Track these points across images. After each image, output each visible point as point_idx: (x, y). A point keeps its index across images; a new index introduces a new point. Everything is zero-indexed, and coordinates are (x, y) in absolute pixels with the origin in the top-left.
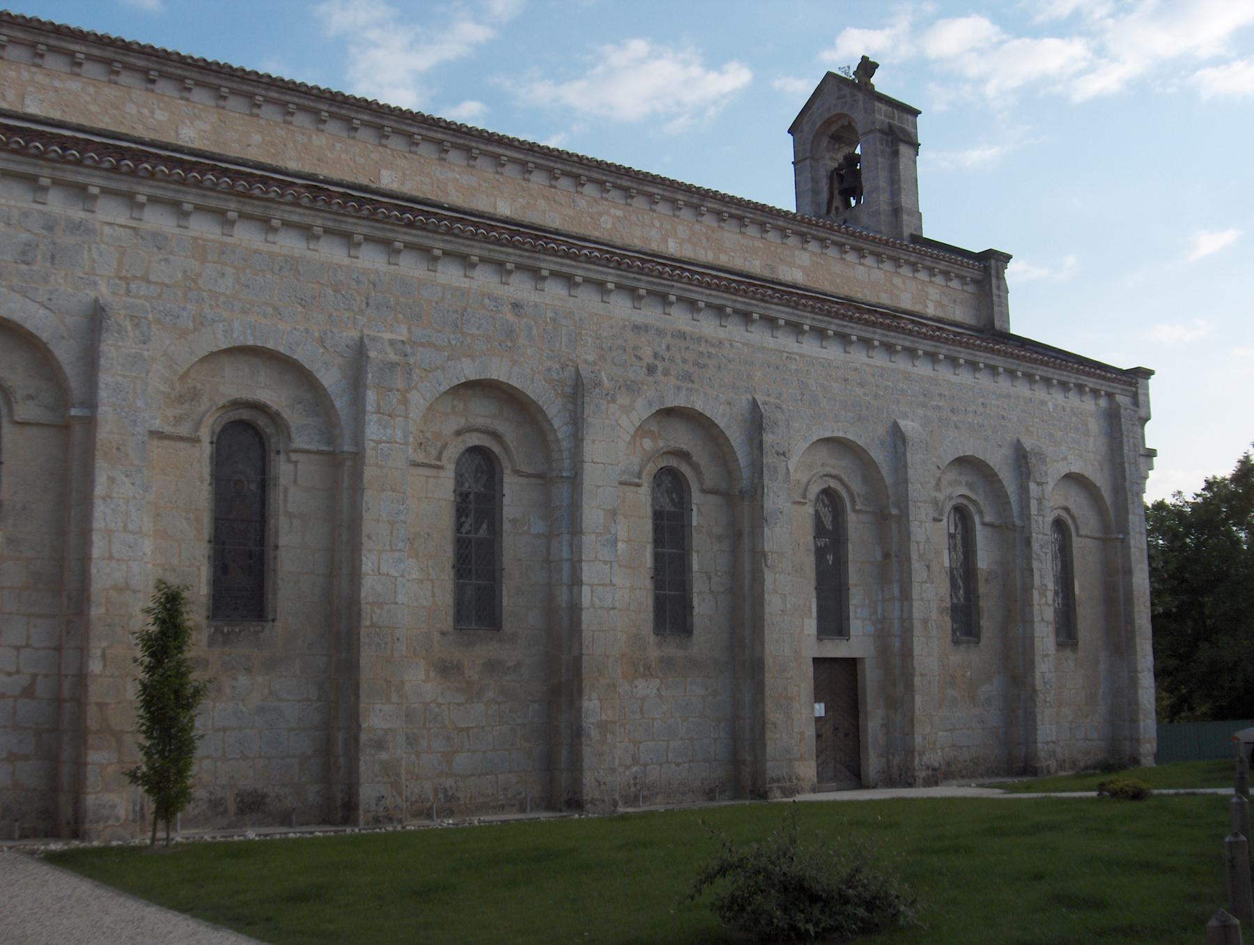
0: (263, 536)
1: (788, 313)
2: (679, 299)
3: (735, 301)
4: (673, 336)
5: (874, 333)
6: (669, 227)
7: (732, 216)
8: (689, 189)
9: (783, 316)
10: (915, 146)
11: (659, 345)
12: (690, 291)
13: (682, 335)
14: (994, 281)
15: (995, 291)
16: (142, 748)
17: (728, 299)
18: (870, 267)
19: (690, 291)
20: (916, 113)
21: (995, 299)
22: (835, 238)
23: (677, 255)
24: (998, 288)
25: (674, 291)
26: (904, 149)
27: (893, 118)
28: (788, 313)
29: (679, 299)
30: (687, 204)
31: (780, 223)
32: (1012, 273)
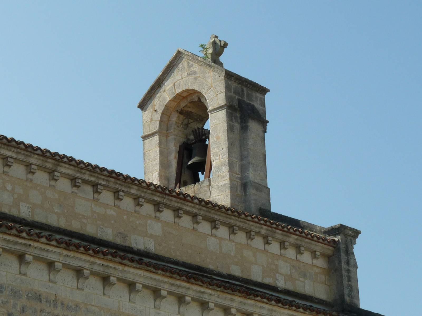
0: (251, 299)
1: (146, 278)
2: (37, 258)
3: (93, 263)
4: (28, 298)
5: (232, 300)
6: (21, 191)
7: (85, 182)
8: (45, 154)
9: (142, 280)
10: (263, 122)
11: (14, 306)
12: (47, 251)
13: (38, 297)
14: (343, 255)
15: (344, 266)
16: (21, 236)
17: (86, 261)
18: (221, 239)
19: (47, 251)
20: (264, 91)
21: (344, 273)
22: (187, 208)
23: (29, 218)
24: (348, 263)
25: (31, 250)
26: (253, 125)
27: (243, 95)
28: (146, 278)
29: (37, 258)
30: (41, 167)
31: (133, 191)
32: (359, 249)
